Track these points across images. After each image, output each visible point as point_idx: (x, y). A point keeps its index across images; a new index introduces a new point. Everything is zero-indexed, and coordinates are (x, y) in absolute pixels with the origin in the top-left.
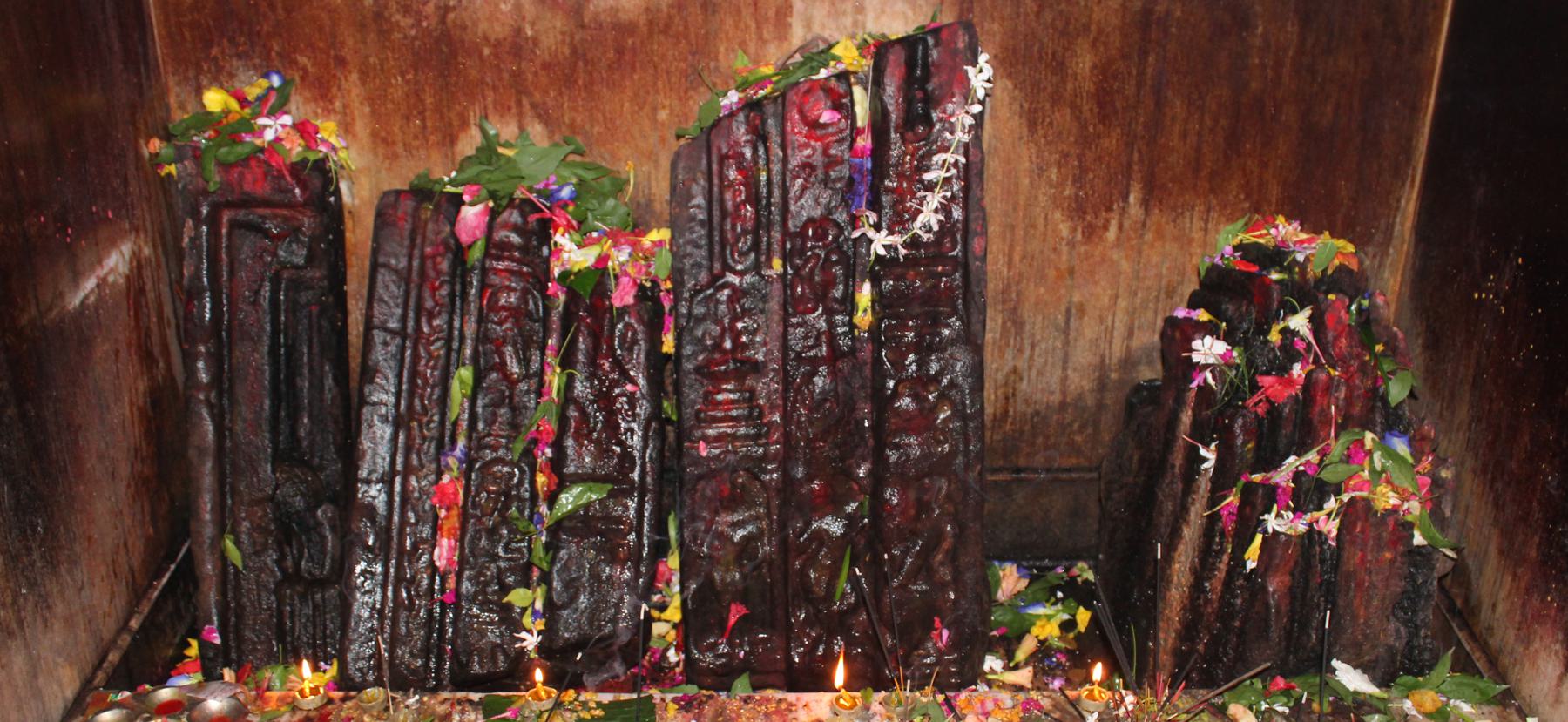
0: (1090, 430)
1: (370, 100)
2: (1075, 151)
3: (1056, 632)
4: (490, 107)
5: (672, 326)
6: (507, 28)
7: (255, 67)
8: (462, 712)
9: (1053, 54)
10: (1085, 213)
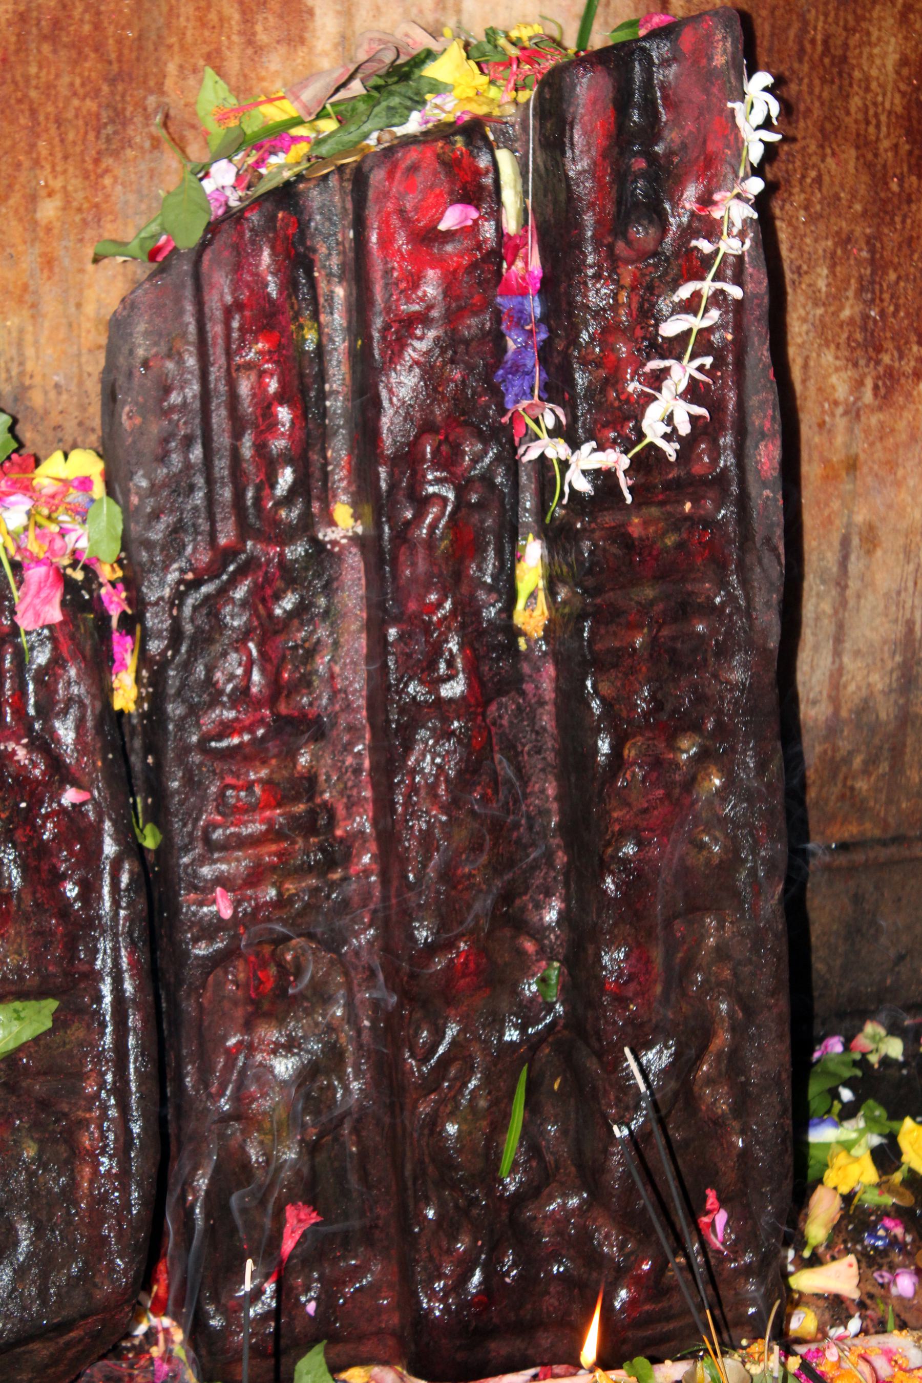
0: (884, 767)
2: (862, 230)
3: (870, 1174)
5: (131, 661)
9: (825, 42)
10: (879, 349)
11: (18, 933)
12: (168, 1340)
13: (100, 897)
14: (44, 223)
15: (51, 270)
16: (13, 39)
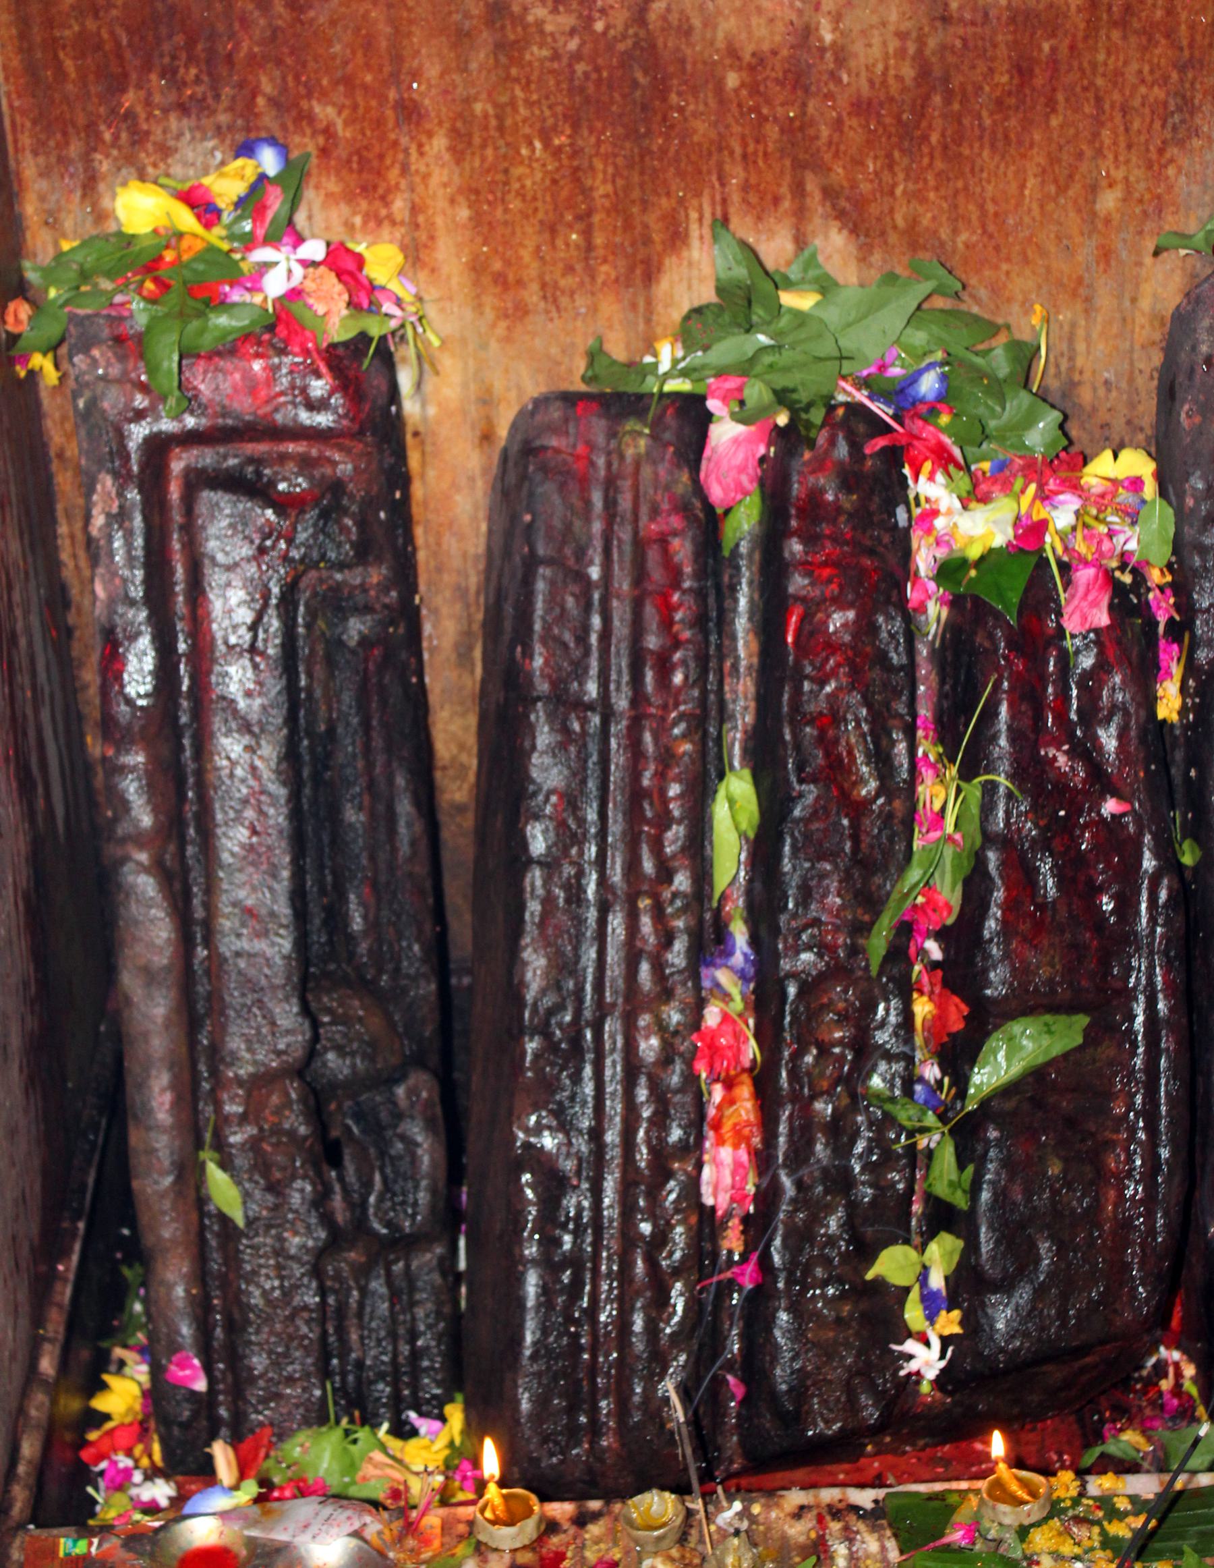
1: (472, 193)
4: (736, 198)
5: (1177, 670)
6: (780, 27)
7: (219, 131)
8: (849, 1536)
11: (1052, 945)
12: (1179, 1375)
13: (1137, 913)
14: (1102, 214)
15: (1108, 263)
16: (1082, 26)
